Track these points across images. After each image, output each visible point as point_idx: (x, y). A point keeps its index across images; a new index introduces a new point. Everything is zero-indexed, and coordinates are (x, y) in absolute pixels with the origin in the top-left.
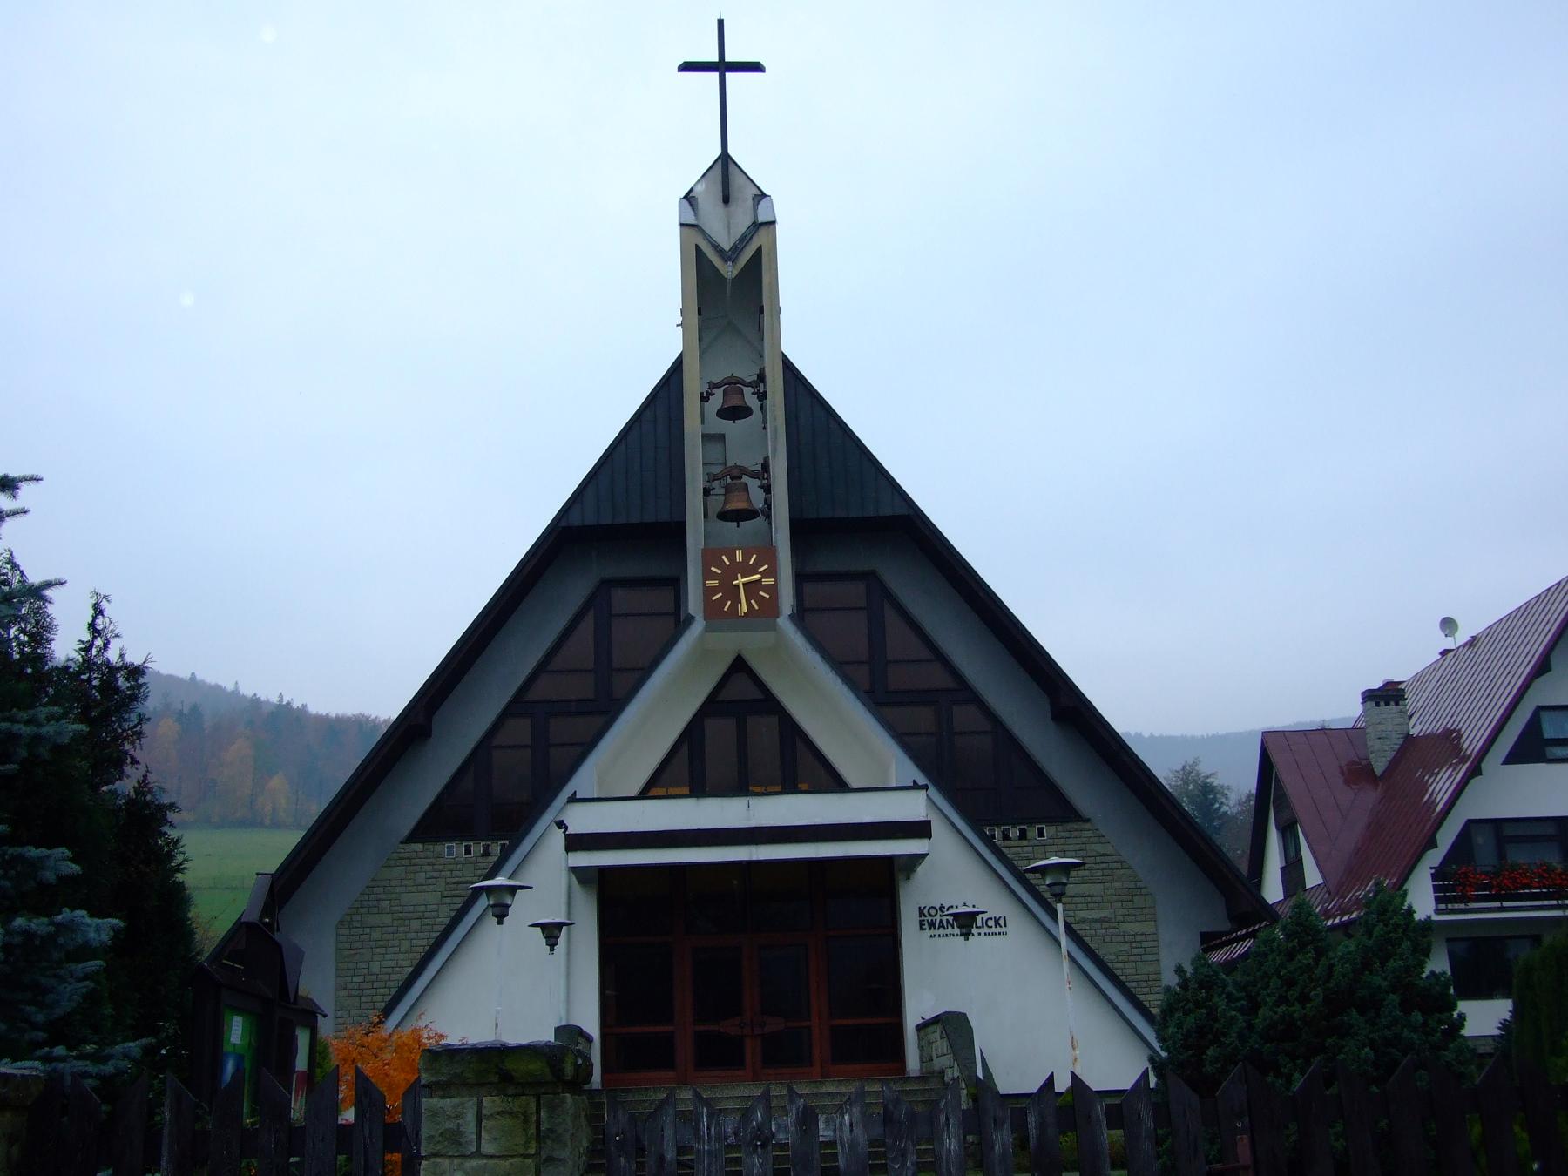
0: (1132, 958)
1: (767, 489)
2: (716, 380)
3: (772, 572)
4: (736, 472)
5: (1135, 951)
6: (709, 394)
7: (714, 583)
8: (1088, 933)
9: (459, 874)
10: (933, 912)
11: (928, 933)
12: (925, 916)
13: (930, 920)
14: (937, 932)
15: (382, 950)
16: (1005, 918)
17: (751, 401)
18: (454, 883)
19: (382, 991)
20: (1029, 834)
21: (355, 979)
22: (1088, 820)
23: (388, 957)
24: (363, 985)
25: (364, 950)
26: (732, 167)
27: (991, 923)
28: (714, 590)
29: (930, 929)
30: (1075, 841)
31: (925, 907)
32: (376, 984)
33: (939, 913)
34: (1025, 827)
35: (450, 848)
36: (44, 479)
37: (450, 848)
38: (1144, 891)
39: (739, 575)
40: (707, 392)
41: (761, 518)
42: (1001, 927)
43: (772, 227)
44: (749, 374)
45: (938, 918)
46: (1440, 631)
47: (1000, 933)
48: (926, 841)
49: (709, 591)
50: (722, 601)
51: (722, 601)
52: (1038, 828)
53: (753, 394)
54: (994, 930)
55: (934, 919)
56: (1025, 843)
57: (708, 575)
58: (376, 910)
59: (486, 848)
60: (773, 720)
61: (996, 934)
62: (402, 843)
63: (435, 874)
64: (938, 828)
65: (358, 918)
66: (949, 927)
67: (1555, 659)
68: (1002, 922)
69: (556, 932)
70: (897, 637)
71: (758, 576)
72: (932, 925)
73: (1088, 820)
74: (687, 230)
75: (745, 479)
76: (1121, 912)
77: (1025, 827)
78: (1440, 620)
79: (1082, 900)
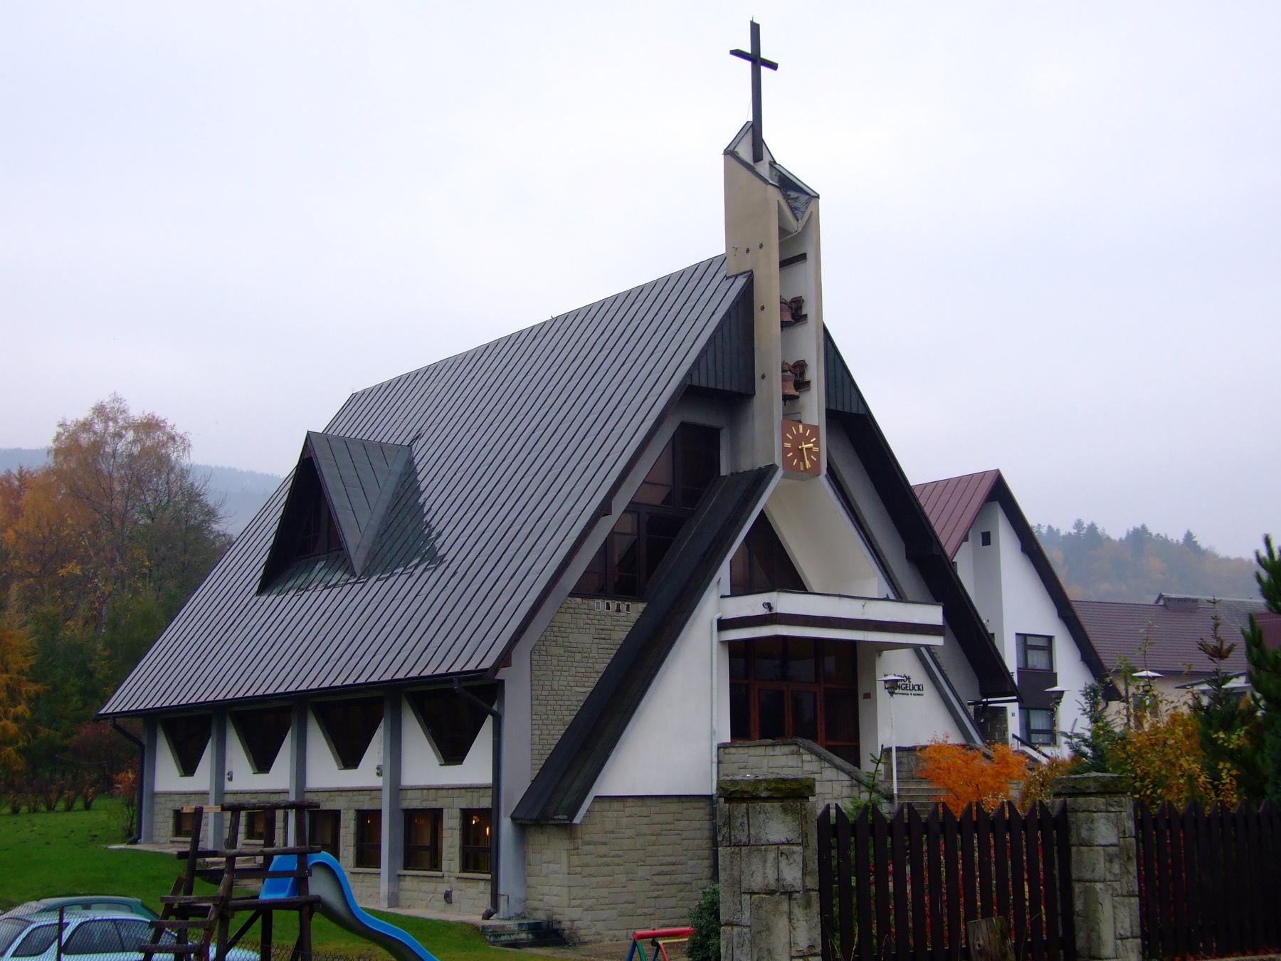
3: (817, 444)
9: (603, 623)
15: (559, 673)
18: (601, 629)
19: (559, 703)
21: (544, 693)
23: (562, 678)
24: (549, 698)
25: (548, 672)
27: (916, 688)
32: (556, 697)
36: (1267, 532)
49: (785, 451)
50: (792, 458)
51: (792, 458)
54: (917, 692)
56: (1189, 664)
57: (785, 439)
58: (554, 644)
59: (608, 604)
63: (590, 622)
65: (544, 648)
68: (921, 688)
71: (811, 445)
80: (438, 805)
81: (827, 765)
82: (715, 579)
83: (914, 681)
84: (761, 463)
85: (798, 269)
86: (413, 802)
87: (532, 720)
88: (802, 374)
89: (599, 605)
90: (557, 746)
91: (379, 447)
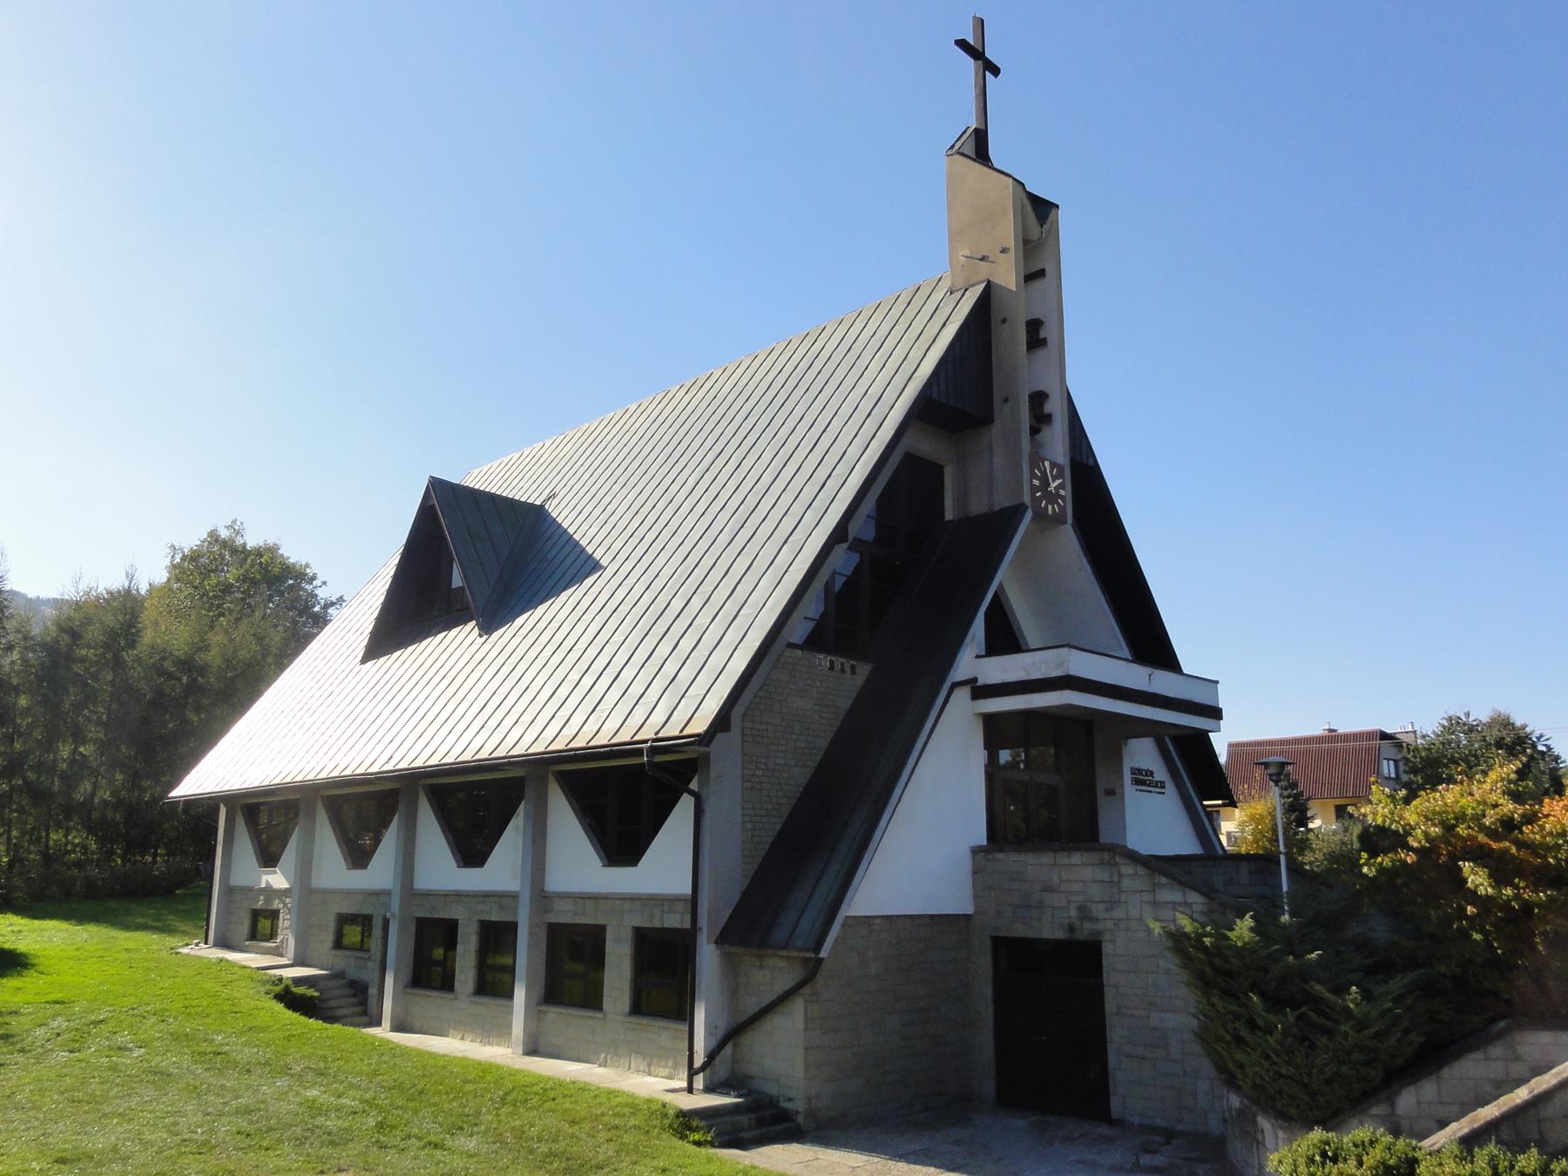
49: (1034, 489)
57: (1033, 476)
80: (600, 922)
81: (1164, 880)
82: (970, 634)
83: (1157, 777)
84: (1002, 501)
85: (1038, 285)
86: (565, 915)
87: (743, 808)
88: (1041, 406)
89: (822, 660)
90: (773, 845)
91: (917, 287)
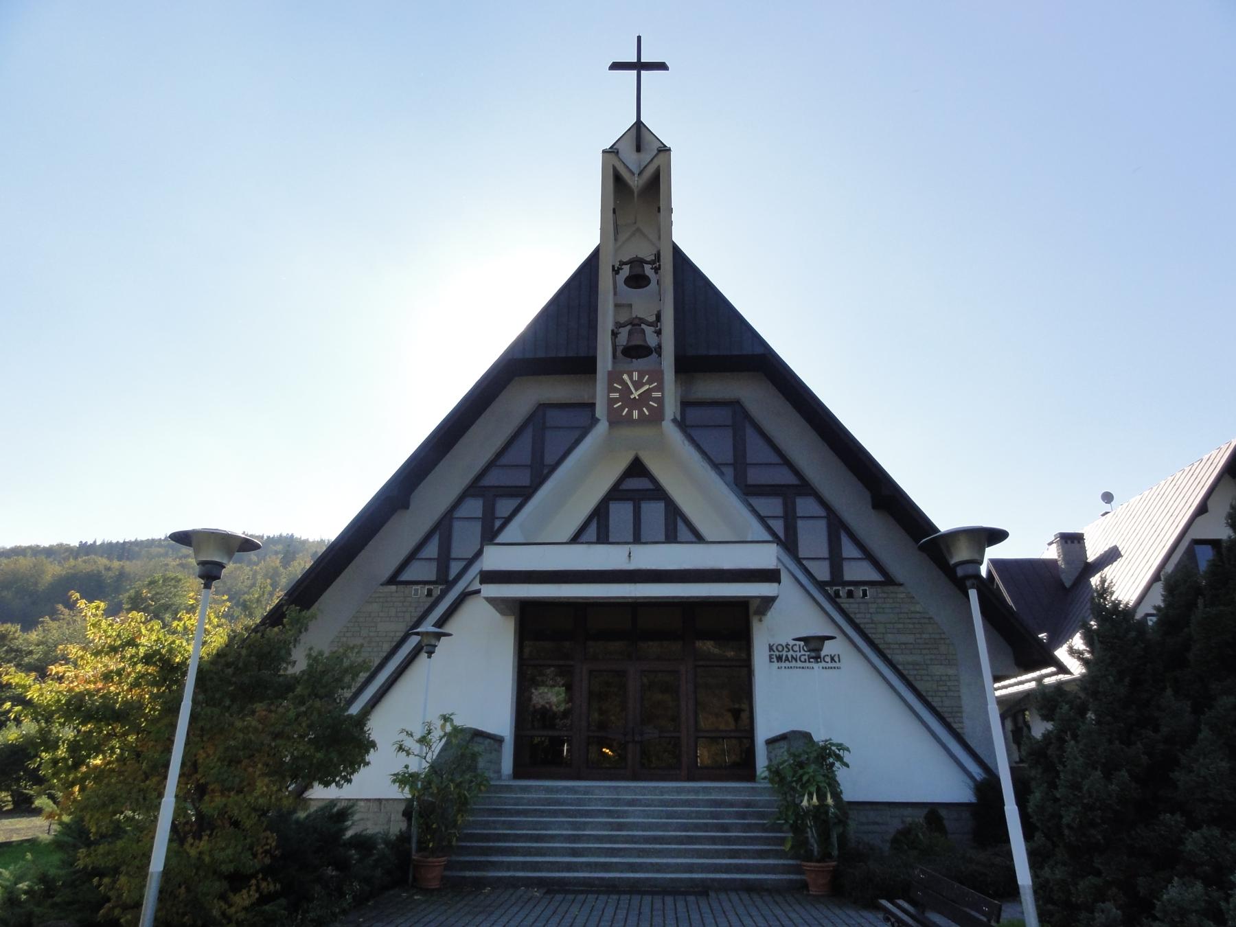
0: (940, 694)
1: (659, 333)
2: (625, 260)
3: (660, 388)
4: (636, 322)
5: (941, 688)
6: (619, 269)
7: (616, 395)
8: (911, 672)
10: (780, 648)
11: (776, 665)
12: (774, 651)
13: (779, 656)
14: (783, 665)
16: (839, 655)
17: (648, 270)
20: (855, 594)
22: (901, 585)
26: (643, 129)
27: (828, 659)
28: (616, 400)
29: (778, 662)
30: (891, 601)
31: (774, 644)
33: (785, 649)
34: (852, 588)
35: (416, 590)
37: (416, 590)
38: (948, 641)
39: (637, 398)
40: (618, 267)
41: (654, 355)
42: (835, 662)
43: (668, 153)
44: (646, 253)
45: (784, 653)
46: (1102, 502)
47: (835, 668)
48: (775, 585)
49: (611, 402)
52: (863, 590)
53: (652, 269)
55: (781, 654)
56: (851, 600)
57: (611, 389)
60: (660, 506)
61: (831, 668)
62: (382, 585)
64: (784, 576)
66: (793, 661)
67: (1210, 504)
68: (836, 659)
69: (433, 642)
70: (756, 450)
72: (779, 659)
73: (901, 585)
74: (607, 155)
75: (643, 326)
76: (928, 657)
77: (852, 588)
78: (1104, 491)
79: (897, 646)
